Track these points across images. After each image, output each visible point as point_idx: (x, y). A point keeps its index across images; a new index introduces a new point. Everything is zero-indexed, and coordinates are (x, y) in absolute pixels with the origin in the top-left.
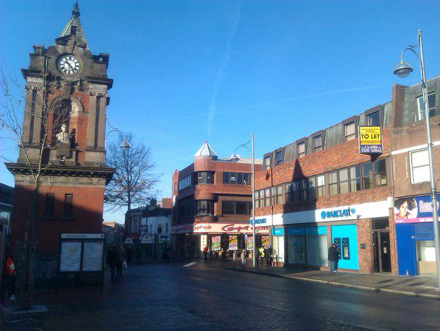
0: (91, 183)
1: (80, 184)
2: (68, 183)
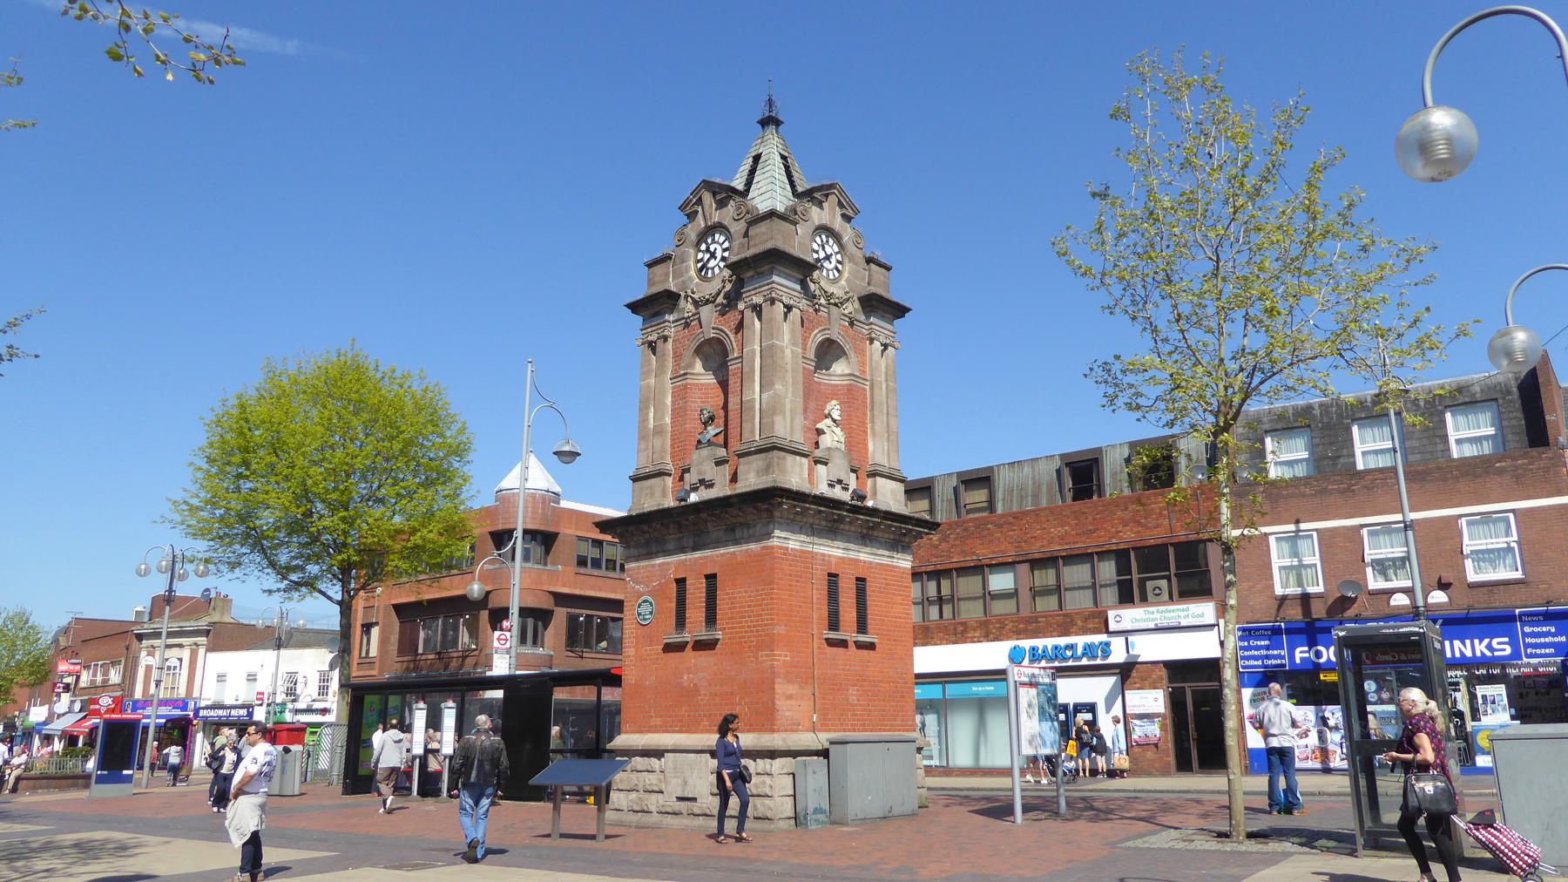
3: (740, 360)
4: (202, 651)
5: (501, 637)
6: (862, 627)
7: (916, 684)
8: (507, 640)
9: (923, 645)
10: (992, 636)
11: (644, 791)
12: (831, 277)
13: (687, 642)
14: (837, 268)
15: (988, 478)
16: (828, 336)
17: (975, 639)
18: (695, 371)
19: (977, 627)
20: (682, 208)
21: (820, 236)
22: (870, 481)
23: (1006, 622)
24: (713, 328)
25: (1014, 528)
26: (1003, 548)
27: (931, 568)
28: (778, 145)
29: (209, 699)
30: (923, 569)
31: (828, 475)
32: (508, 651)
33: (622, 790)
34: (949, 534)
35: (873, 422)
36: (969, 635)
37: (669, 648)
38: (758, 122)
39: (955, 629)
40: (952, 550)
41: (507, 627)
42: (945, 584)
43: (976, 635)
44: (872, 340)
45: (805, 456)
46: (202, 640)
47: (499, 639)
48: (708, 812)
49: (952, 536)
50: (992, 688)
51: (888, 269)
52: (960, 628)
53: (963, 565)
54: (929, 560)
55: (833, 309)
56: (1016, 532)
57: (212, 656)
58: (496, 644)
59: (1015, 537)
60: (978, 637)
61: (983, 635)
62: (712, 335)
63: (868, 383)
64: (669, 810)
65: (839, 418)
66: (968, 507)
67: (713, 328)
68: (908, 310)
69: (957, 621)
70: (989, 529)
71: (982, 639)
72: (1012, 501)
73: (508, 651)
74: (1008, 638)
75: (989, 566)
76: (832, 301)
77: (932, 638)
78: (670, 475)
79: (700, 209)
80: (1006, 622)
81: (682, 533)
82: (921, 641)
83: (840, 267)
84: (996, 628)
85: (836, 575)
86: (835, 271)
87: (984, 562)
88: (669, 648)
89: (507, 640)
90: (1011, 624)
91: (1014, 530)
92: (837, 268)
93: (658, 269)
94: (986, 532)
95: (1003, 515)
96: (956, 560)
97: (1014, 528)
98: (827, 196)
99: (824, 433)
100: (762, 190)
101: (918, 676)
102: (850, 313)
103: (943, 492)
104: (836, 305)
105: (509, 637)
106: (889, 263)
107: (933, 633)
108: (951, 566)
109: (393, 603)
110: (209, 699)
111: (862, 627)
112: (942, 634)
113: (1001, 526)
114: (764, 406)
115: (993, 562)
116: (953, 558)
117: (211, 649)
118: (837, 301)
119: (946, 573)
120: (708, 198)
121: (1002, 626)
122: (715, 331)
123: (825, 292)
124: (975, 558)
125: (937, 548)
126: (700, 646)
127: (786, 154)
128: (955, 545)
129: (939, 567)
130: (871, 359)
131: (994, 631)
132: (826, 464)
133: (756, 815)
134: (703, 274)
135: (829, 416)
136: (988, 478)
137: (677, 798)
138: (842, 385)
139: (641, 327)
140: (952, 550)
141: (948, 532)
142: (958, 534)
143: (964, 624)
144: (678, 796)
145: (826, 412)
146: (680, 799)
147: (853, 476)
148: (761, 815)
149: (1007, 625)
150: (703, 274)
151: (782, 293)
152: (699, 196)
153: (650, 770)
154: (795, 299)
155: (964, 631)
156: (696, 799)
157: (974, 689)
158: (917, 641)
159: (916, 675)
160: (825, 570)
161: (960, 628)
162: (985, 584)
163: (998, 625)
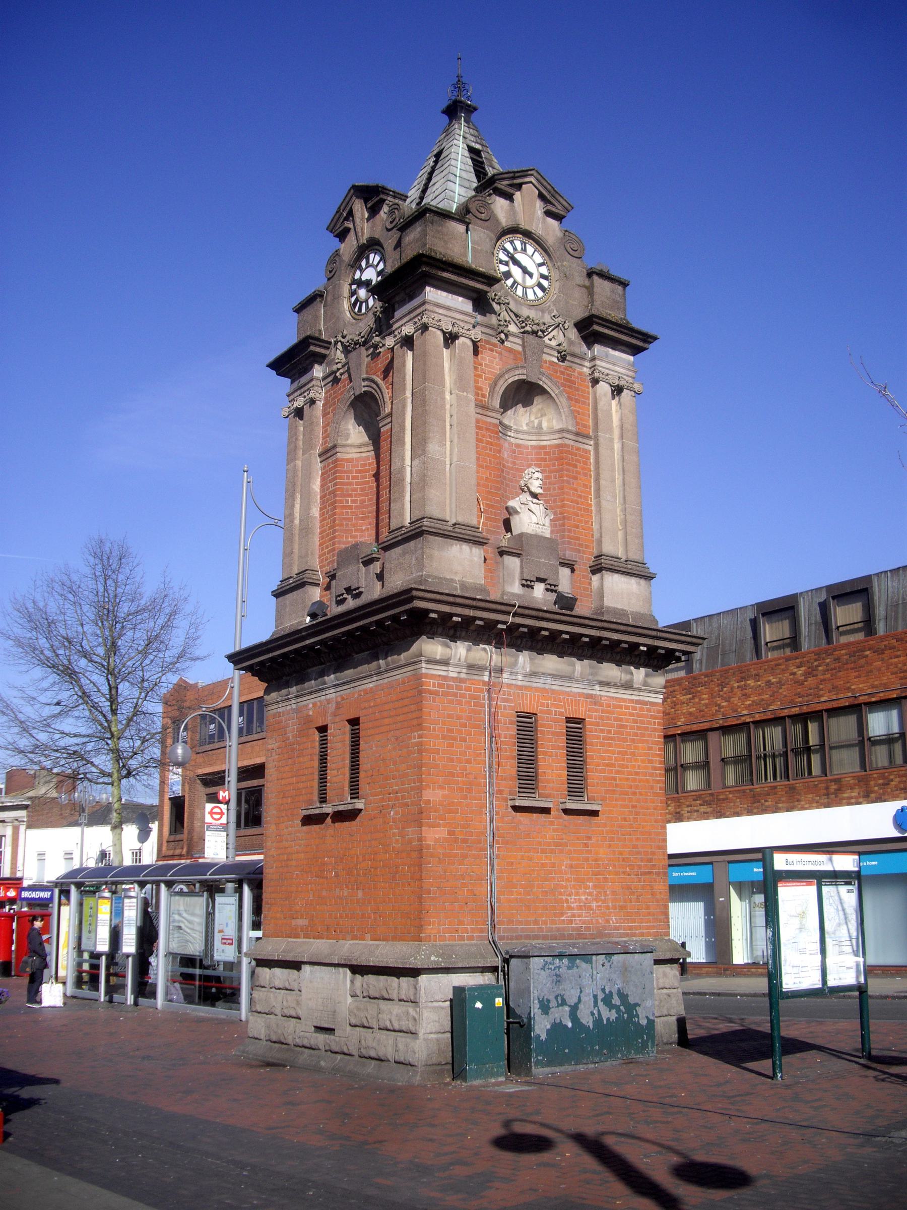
0: (628, 686)
1: (603, 684)
2: (569, 678)
3: (389, 420)
4: (22, 828)
5: (215, 810)
6: (576, 786)
7: (670, 866)
8: (222, 814)
9: (788, 811)
10: (873, 795)
11: (282, 1016)
12: (531, 296)
13: (328, 814)
14: (540, 286)
15: (866, 590)
16: (525, 377)
17: (853, 801)
18: (349, 442)
19: (855, 785)
20: (330, 228)
21: (512, 242)
22: (596, 578)
23: (892, 777)
24: (364, 380)
25: (899, 653)
26: (885, 680)
27: (796, 711)
28: (467, 136)
29: (31, 879)
30: (786, 712)
31: (522, 573)
32: (225, 827)
33: (260, 1013)
34: (817, 666)
35: (598, 496)
36: (845, 795)
37: (308, 820)
38: (443, 112)
39: (827, 788)
40: (821, 687)
41: (224, 798)
42: (813, 727)
43: (853, 794)
44: (595, 382)
45: (479, 542)
46: (22, 813)
47: (211, 813)
48: (345, 1050)
49: (820, 668)
50: (695, 874)
51: (624, 284)
52: (833, 787)
53: (835, 705)
54: (792, 701)
55: (531, 338)
56: (902, 658)
57: (31, 832)
58: (208, 819)
59: (900, 665)
60: (856, 798)
61: (862, 794)
62: (364, 389)
63: (592, 443)
64: (306, 1043)
65: (539, 491)
66: (841, 629)
67: (364, 380)
68: (655, 338)
69: (829, 777)
70: (867, 656)
71: (861, 800)
72: (896, 619)
73: (225, 827)
74: (894, 798)
75: (867, 704)
76: (528, 328)
77: (798, 801)
78: (317, 585)
79: (351, 226)
80: (892, 777)
81: (322, 664)
82: (785, 805)
83: (545, 283)
84: (879, 785)
85: (530, 715)
86: (537, 289)
87: (862, 699)
88: (308, 820)
89: (222, 814)
90: (898, 779)
91: (899, 656)
92: (540, 286)
93: (308, 313)
94: (862, 661)
95: (882, 638)
96: (826, 698)
97: (899, 653)
98: (519, 187)
99: (517, 512)
100: (437, 193)
101: (671, 856)
102: (559, 345)
103: (807, 613)
104: (535, 333)
105: (225, 811)
106: (623, 276)
107: (800, 794)
108: (819, 707)
109: (200, 771)
110: (31, 879)
111: (576, 786)
112: (811, 796)
113: (882, 652)
114: (415, 475)
115: (873, 699)
116: (822, 696)
117: (30, 826)
118: (535, 328)
119: (816, 715)
120: (360, 209)
121: (886, 782)
122: (366, 383)
123: (516, 316)
124: (850, 694)
125: (802, 684)
126: (342, 816)
127: (478, 146)
128: (824, 680)
129: (805, 709)
130: (596, 408)
131: (876, 788)
132: (518, 555)
133: (397, 1058)
134: (356, 310)
135: (523, 490)
136: (866, 590)
137: (316, 1027)
138: (550, 446)
139: (288, 391)
140: (821, 687)
141: (816, 664)
142: (827, 665)
143: (837, 781)
144: (315, 1025)
145: (522, 483)
146: (319, 1029)
147: (565, 572)
148: (402, 1059)
149: (892, 780)
150: (356, 310)
151: (441, 317)
152: (348, 208)
153: (289, 988)
154: (462, 324)
155: (839, 790)
156: (334, 1030)
157: (674, 874)
158: (780, 805)
159: (669, 855)
160: (511, 708)
161: (833, 787)
162: (862, 726)
163: (881, 781)
